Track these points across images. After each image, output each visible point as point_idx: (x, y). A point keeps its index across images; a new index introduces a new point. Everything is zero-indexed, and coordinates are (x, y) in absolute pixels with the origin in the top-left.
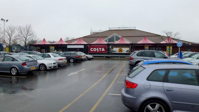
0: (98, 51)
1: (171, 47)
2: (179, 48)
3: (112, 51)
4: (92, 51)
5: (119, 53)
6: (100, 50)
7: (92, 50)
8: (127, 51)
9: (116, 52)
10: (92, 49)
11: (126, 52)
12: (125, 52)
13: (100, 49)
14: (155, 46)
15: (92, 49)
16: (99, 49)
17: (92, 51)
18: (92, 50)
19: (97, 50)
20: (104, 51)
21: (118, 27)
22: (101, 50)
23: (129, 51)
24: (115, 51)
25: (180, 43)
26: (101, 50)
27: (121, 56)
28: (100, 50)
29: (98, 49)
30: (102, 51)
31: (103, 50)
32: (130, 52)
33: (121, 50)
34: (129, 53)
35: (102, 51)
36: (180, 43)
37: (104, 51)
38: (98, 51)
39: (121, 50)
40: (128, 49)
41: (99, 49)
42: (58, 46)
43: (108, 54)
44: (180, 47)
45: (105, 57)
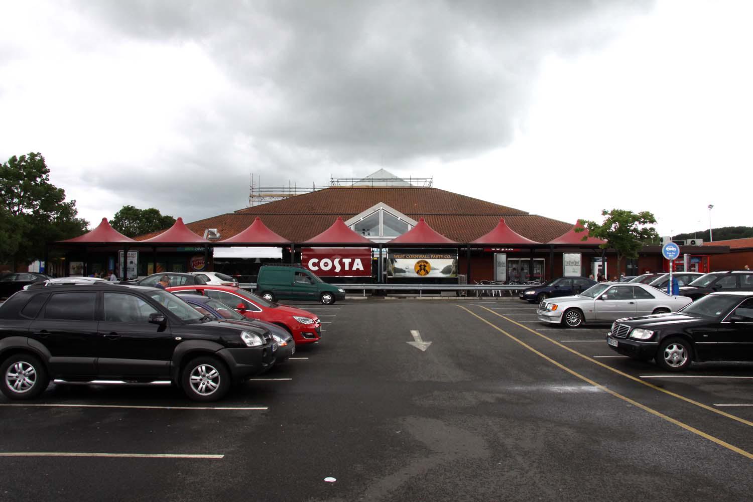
0: (338, 269)
1: (136, 254)
2: (671, 264)
3: (390, 268)
4: (316, 268)
5: (416, 275)
6: (347, 268)
7: (314, 265)
8: (446, 270)
9: (408, 275)
10: (316, 260)
11: (443, 272)
12: (438, 274)
13: (347, 261)
14: (529, 250)
15: (316, 260)
16: (342, 264)
17: (316, 268)
18: (314, 265)
19: (334, 267)
20: (361, 268)
21: (365, 176)
22: (351, 265)
23: (454, 269)
24: (404, 272)
25: (670, 249)
26: (351, 265)
27: (421, 287)
28: (347, 268)
29: (336, 261)
30: (354, 268)
31: (358, 265)
32: (454, 273)
33: (423, 267)
34: (454, 276)
35: (354, 268)
36: (673, 249)
37: (361, 268)
38: (338, 269)
39: (423, 267)
40: (449, 262)
41: (342, 264)
42: (159, 249)
43: (373, 281)
44: (673, 261)
45: (368, 291)
